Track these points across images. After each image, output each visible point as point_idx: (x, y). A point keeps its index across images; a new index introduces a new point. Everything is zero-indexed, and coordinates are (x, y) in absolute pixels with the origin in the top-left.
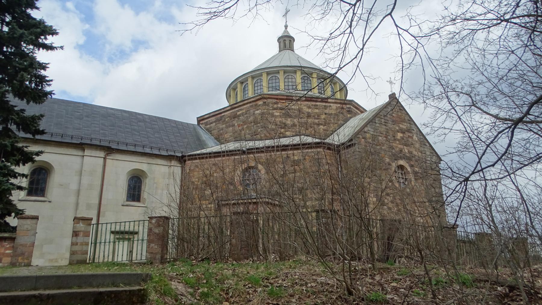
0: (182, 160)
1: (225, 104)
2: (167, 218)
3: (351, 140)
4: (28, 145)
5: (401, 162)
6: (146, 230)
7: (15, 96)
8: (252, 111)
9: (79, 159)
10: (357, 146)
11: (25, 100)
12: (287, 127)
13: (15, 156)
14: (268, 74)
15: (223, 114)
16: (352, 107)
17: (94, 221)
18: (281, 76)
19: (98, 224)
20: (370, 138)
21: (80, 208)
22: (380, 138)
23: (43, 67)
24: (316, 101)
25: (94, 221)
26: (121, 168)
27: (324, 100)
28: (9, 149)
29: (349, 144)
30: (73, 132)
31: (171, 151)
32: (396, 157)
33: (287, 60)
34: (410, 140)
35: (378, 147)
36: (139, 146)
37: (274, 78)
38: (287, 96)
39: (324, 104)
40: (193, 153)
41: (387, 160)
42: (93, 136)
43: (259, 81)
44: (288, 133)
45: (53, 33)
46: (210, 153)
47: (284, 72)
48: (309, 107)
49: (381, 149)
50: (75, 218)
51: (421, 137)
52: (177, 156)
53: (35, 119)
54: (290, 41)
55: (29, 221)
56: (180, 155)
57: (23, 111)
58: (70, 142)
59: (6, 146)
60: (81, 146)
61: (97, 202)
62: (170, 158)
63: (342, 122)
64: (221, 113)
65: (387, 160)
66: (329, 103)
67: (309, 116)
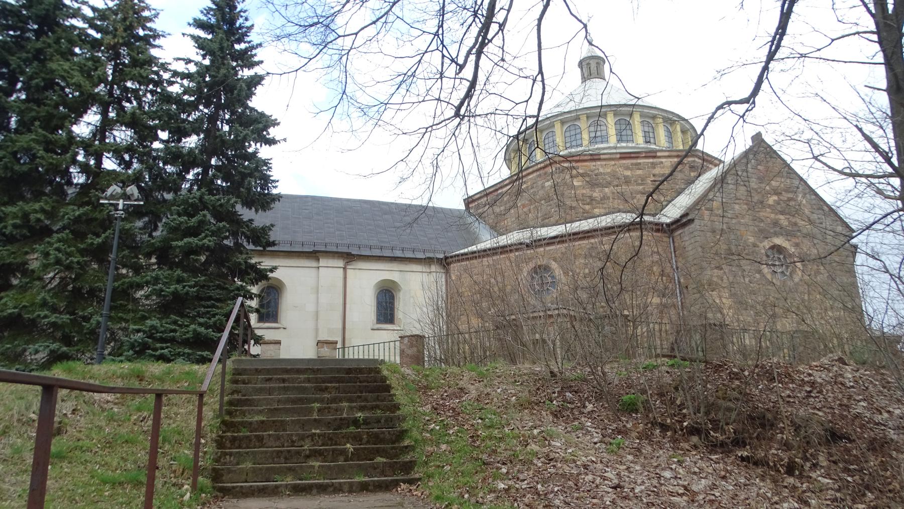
0: (445, 263)
1: (505, 173)
2: (420, 338)
3: (685, 215)
4: (260, 260)
5: (778, 241)
6: (398, 351)
7: (243, 205)
8: (540, 183)
9: (314, 271)
10: (697, 222)
11: (253, 209)
12: (594, 202)
13: (249, 274)
14: (563, 122)
15: (500, 191)
16: (697, 159)
17: (339, 345)
18: (583, 124)
19: (344, 348)
20: (718, 209)
21: (320, 332)
22: (737, 207)
23: (266, 163)
24: (637, 157)
25: (339, 345)
26: (366, 279)
27: (652, 154)
28: (243, 267)
29: (681, 223)
30: (303, 238)
31: (429, 251)
32: (765, 234)
33: (595, 95)
34: (792, 203)
35: (734, 221)
36: (386, 248)
37: (572, 128)
38: (591, 155)
39: (651, 160)
40: (462, 251)
41: (752, 240)
42: (327, 240)
43: (550, 134)
44: (597, 211)
45: (275, 123)
46: (485, 251)
47: (588, 117)
48: (627, 168)
49: (739, 223)
50: (319, 342)
51: (813, 197)
52: (438, 259)
53: (265, 230)
54: (597, 63)
55: (272, 347)
56: (441, 256)
57: (251, 221)
58: (300, 250)
59: (240, 264)
60: (314, 255)
61: (340, 326)
62: (428, 261)
63: (683, 187)
64: (497, 190)
65: (752, 240)
66: (660, 157)
67: (627, 181)
